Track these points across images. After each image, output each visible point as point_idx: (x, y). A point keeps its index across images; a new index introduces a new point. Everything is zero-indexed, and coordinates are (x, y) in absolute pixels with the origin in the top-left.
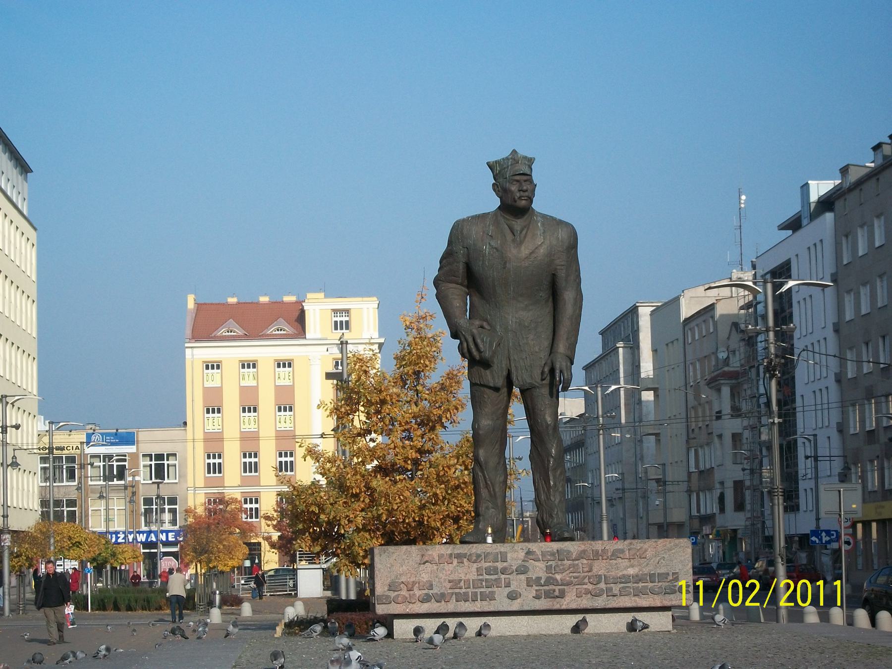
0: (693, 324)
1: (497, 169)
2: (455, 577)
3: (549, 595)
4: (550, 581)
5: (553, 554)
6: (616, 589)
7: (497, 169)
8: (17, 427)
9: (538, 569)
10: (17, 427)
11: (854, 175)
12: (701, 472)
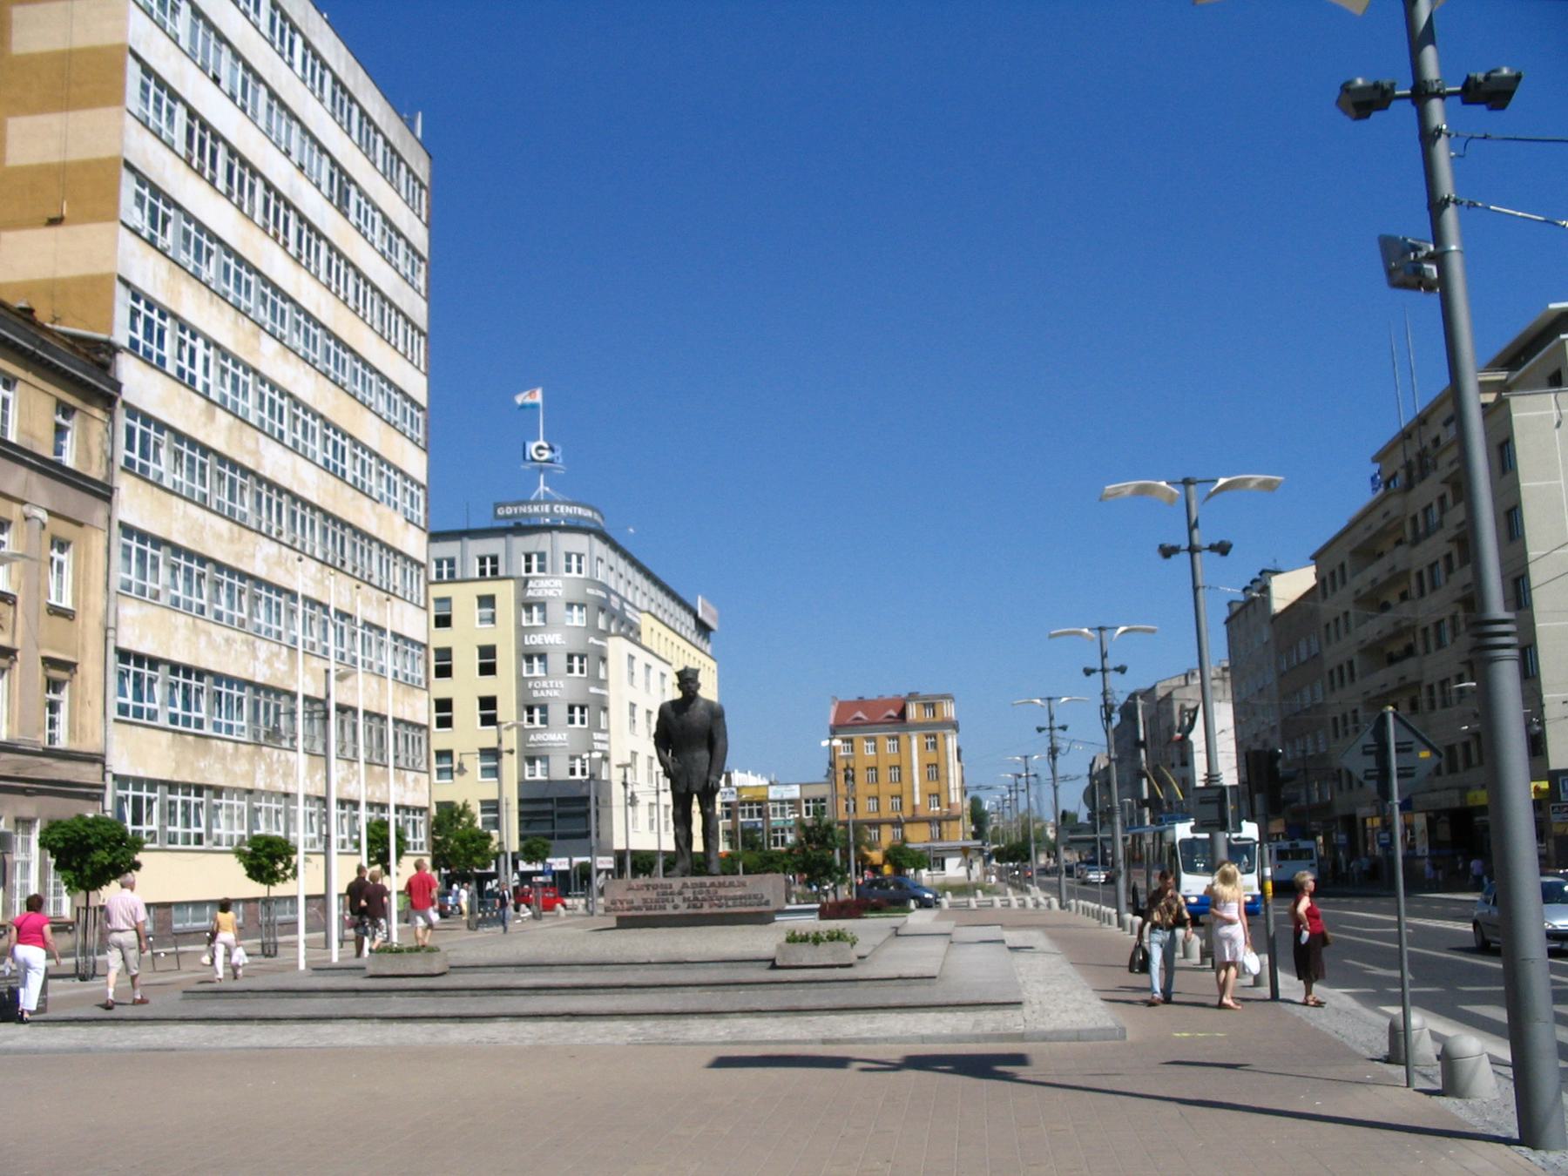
1: (680, 675)
3: (695, 907)
4: (696, 899)
7: (680, 675)
9: (689, 894)
11: (1236, 607)
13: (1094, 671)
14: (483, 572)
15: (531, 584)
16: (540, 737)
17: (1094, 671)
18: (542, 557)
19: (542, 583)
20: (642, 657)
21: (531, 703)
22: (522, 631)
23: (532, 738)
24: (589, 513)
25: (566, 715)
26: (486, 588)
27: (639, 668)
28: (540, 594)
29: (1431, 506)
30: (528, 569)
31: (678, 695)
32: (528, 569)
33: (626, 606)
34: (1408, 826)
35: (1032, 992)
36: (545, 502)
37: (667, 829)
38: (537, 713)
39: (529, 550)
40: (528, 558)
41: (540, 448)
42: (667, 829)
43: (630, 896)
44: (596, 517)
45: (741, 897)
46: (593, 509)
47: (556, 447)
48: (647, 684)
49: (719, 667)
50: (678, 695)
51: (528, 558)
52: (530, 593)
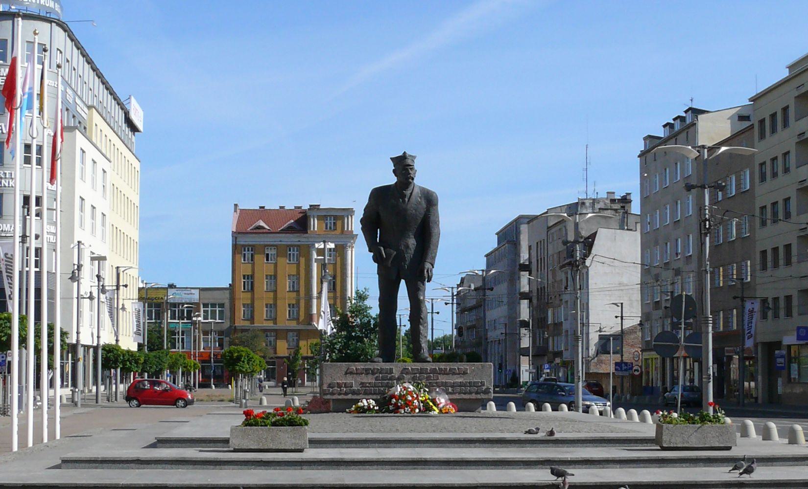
0: (553, 230)
2: (364, 381)
6: (458, 389)
8: (126, 286)
10: (126, 286)
12: (555, 324)
27: (89, 163)
31: (392, 180)
33: (78, 101)
34: (459, 393)
43: (350, 380)
44: (57, 8)
45: (461, 385)
50: (392, 180)
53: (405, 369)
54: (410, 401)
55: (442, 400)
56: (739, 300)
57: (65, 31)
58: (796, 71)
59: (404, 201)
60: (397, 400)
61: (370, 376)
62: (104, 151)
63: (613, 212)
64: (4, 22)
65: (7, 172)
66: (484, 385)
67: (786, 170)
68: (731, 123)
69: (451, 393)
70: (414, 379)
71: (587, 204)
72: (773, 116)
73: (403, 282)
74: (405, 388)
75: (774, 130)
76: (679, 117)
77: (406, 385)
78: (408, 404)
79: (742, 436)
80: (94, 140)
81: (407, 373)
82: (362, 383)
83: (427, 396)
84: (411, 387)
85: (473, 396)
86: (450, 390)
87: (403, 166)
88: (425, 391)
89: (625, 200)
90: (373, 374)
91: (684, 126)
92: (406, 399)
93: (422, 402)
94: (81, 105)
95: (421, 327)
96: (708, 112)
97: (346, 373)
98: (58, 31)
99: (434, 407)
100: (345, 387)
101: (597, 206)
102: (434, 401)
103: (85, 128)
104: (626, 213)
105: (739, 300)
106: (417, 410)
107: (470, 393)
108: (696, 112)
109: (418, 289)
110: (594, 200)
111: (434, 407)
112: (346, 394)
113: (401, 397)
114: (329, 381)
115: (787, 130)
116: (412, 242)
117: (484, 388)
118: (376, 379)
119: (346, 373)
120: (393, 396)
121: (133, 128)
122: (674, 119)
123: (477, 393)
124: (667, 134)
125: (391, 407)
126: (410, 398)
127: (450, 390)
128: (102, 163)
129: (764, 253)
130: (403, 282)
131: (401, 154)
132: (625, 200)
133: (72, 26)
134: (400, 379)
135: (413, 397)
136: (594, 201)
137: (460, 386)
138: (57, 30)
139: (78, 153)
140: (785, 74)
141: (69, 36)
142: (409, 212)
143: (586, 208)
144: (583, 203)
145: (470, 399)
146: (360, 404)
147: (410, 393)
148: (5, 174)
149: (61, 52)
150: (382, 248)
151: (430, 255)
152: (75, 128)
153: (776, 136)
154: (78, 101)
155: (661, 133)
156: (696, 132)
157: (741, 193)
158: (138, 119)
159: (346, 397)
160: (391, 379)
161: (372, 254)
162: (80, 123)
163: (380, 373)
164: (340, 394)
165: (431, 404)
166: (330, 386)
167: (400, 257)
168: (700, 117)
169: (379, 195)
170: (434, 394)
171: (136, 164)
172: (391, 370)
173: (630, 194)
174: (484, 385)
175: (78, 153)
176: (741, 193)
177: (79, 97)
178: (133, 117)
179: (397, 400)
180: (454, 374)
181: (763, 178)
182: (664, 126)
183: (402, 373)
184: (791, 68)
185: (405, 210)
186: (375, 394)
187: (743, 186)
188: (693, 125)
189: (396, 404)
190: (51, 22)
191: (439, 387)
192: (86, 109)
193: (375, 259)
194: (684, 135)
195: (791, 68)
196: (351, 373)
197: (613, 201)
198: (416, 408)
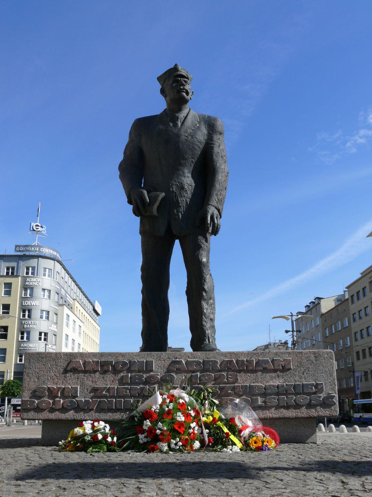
2: (100, 384)
5: (198, 363)
6: (274, 400)
13: (289, 331)
14: (8, 273)
15: (28, 279)
16: (25, 345)
17: (289, 331)
18: (33, 268)
19: (33, 280)
20: (72, 317)
21: (23, 330)
22: (23, 299)
23: (22, 345)
24: (55, 253)
25: (38, 336)
26: (8, 280)
27: (71, 322)
28: (31, 284)
29: (359, 291)
30: (27, 273)
31: (157, 105)
32: (27, 273)
33: (67, 295)
34: (278, 407)
35: (107, 428)
36: (37, 246)
37: (352, 383)
38: (27, 313)
39: (27, 265)
40: (28, 269)
41: (37, 225)
42: (352, 383)
44: (58, 255)
45: (280, 391)
46: (57, 252)
47: (44, 226)
48: (74, 329)
49: (101, 329)
51: (28, 269)
52: (27, 283)
53: (174, 362)
54: (181, 424)
55: (247, 421)
56: (352, 373)
57: (61, 265)
58: (363, 275)
59: (175, 125)
60: (154, 423)
61: (109, 377)
62: (81, 319)
63: (282, 347)
64: (34, 260)
65: (33, 322)
66: (321, 391)
67: (360, 318)
68: (335, 302)
69: (260, 408)
70: (191, 382)
71: (272, 345)
72: (358, 293)
73: (177, 242)
74: (172, 398)
75: (358, 299)
76: (312, 302)
77: (176, 392)
78: (176, 430)
79: (319, 431)
80: (75, 313)
81: (178, 371)
82: (95, 390)
83: (217, 414)
84: (187, 398)
85: (303, 412)
86: (260, 401)
87: (173, 84)
88: (212, 404)
89: (286, 343)
90: (116, 371)
91: (315, 305)
92: (173, 421)
93: (207, 425)
94: (69, 297)
95: (204, 304)
96: (325, 298)
97: (66, 371)
98: (57, 264)
99: (232, 437)
100: (63, 396)
101: (276, 345)
102: (230, 423)
103: (72, 308)
104: (288, 347)
105: (352, 373)
106: (197, 445)
107: (297, 406)
108: (319, 299)
109: (199, 247)
110: (274, 343)
111: (232, 437)
112: (64, 410)
113: (164, 415)
114: (33, 386)
115: (366, 298)
116: (188, 181)
117: (323, 395)
118: (122, 382)
119: (66, 371)
120: (147, 415)
121: (97, 314)
122: (310, 303)
123: (310, 406)
124: (307, 310)
125: (142, 438)
126: (181, 418)
127: (260, 401)
128: (78, 322)
129: (358, 353)
130: (177, 242)
131: (172, 66)
132: (286, 343)
133: (63, 263)
134: (165, 382)
135: (187, 415)
136: (274, 344)
137: (278, 394)
138: (57, 264)
139: (65, 316)
140: (360, 276)
141: (63, 267)
142: (183, 138)
143: (272, 346)
144: (270, 344)
145: (296, 418)
146: (78, 431)
147: (182, 408)
148: (32, 322)
149: (59, 273)
150: (145, 192)
151: (214, 201)
152: (64, 305)
153: (360, 301)
154: (67, 295)
155: (304, 310)
156: (320, 307)
157: (344, 328)
158: (99, 309)
159: (63, 416)
160: (147, 382)
161: (132, 206)
162: (65, 302)
163: (129, 370)
164: (52, 410)
165: (226, 430)
166: (35, 394)
167: (170, 203)
168: (321, 300)
169: (143, 126)
170: (229, 410)
171: (99, 328)
172: (149, 364)
173: (287, 341)
174: (321, 391)
175: (65, 316)
176: (344, 328)
177: (68, 294)
178: (96, 308)
179: (154, 423)
180: (265, 370)
181: (354, 320)
182: (305, 307)
183: (169, 371)
184: (361, 274)
185: (178, 136)
186: (110, 410)
187: (344, 325)
188: (319, 304)
189: (151, 431)
190: (54, 260)
191: (239, 396)
192: (72, 300)
193: (137, 212)
194: (315, 308)
195: (361, 274)
196: (75, 370)
197: (281, 343)
198: (193, 440)
